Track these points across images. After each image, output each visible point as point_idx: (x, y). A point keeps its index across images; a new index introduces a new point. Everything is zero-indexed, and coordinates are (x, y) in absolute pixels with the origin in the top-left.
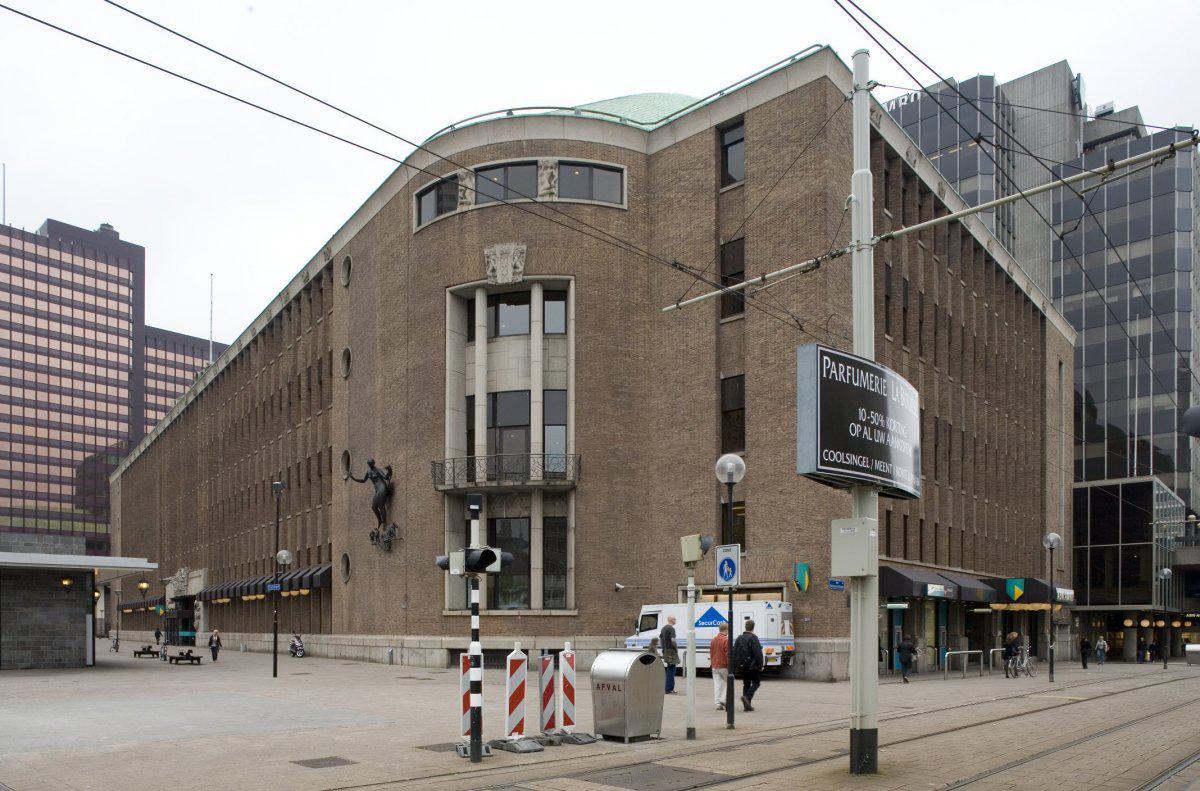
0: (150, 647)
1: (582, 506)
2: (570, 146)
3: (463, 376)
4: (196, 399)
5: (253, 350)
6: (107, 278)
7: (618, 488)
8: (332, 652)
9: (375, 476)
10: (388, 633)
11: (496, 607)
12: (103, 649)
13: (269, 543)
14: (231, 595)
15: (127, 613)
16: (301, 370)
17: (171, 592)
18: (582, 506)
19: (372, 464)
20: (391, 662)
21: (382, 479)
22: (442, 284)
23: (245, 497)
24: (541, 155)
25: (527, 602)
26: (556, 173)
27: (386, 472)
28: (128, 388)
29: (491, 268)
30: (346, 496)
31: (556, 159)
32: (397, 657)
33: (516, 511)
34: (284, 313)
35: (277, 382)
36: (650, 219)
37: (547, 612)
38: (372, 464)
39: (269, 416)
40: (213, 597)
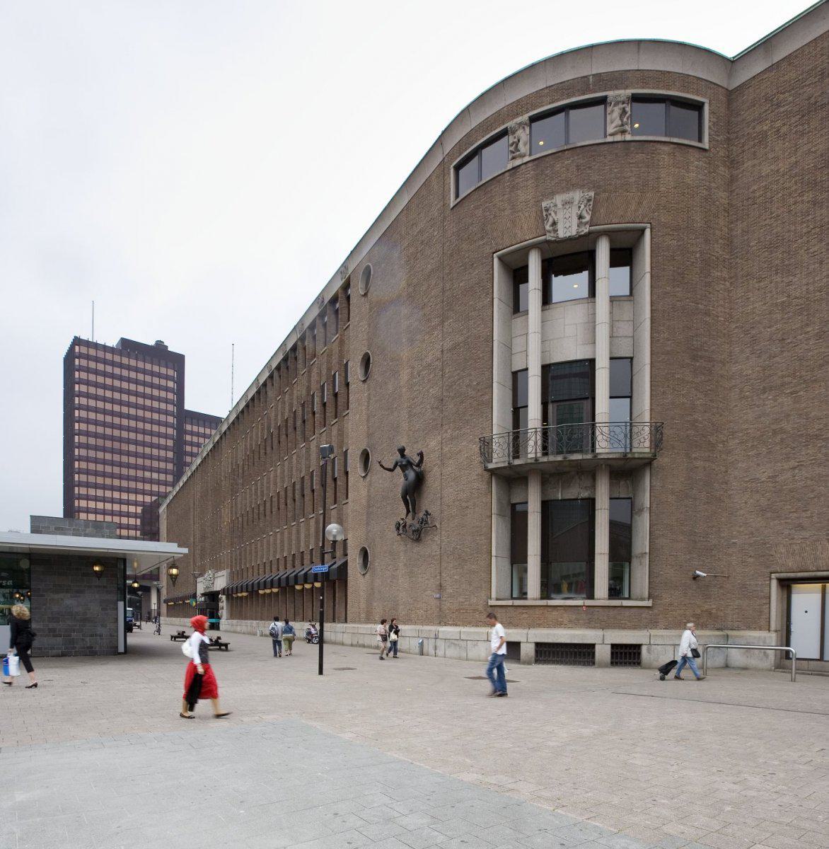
0: (184, 632)
2: (644, 76)
4: (221, 438)
5: (269, 384)
6: (159, 376)
7: (698, 463)
8: (347, 639)
9: (406, 465)
10: (415, 623)
11: (549, 598)
12: (144, 635)
13: (283, 546)
14: (250, 589)
15: (171, 605)
16: (315, 387)
17: (200, 589)
19: (402, 451)
20: (422, 653)
22: (488, 250)
23: (262, 508)
24: (611, 89)
25: (591, 596)
26: (628, 109)
27: (417, 459)
28: (173, 451)
29: (551, 220)
30: (364, 493)
31: (629, 92)
32: (429, 647)
34: (299, 343)
35: (291, 405)
36: (732, 163)
37: (544, 602)
38: (402, 451)
39: (284, 436)
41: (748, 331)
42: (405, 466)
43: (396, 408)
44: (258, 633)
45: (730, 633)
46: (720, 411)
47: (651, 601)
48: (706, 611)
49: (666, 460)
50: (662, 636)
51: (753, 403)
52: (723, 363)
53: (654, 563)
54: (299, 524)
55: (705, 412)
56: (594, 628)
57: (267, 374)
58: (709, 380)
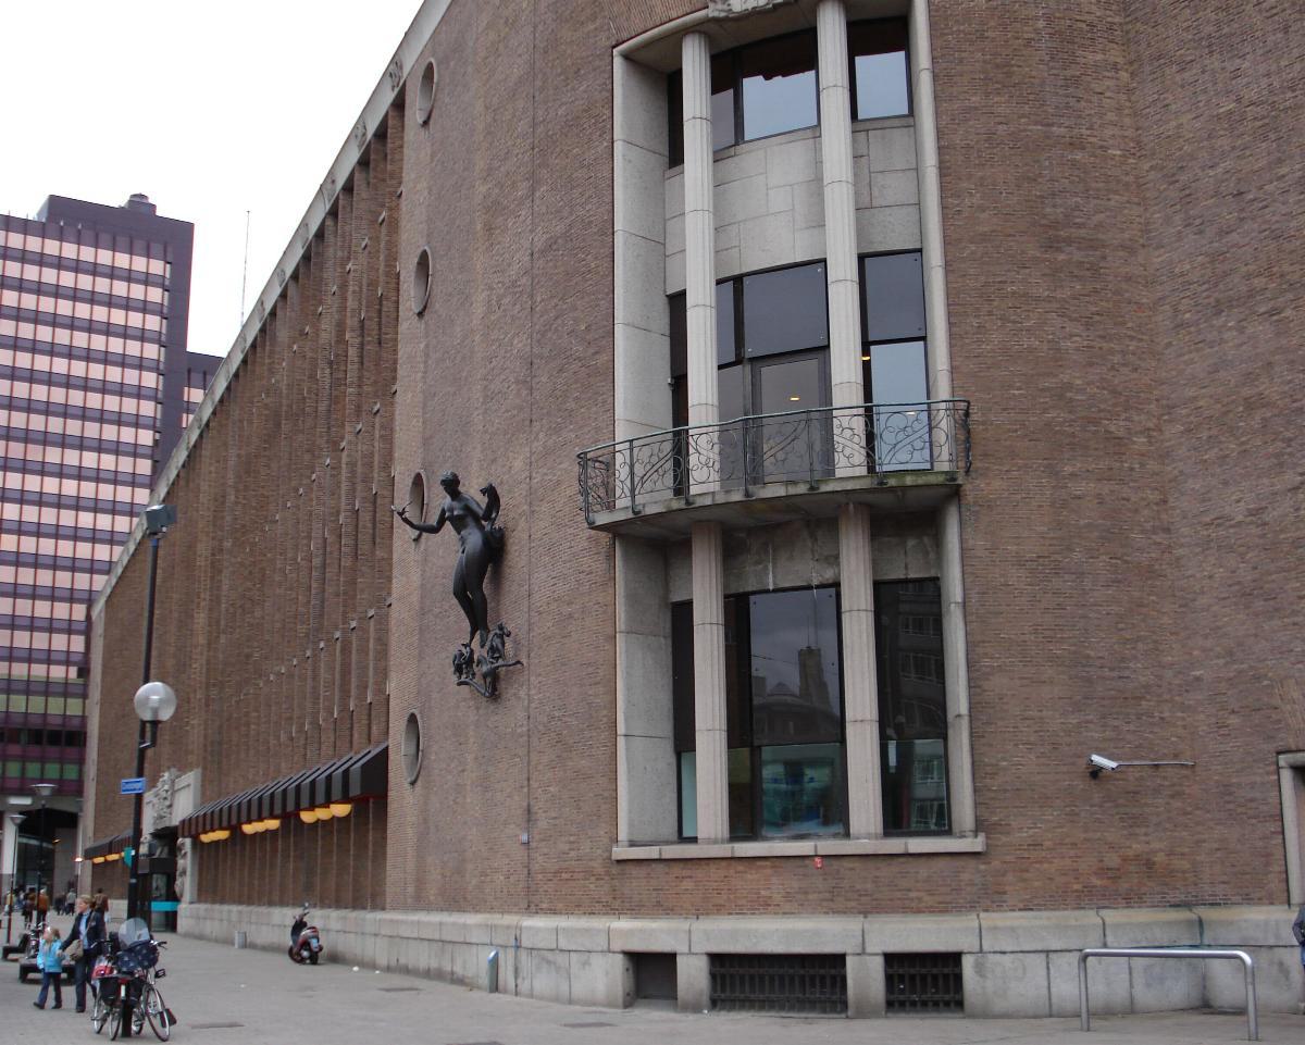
1: (979, 543)
3: (660, 246)
7: (1079, 487)
8: (381, 953)
9: (462, 518)
10: (492, 910)
18: (979, 543)
21: (477, 519)
27: (483, 501)
28: (151, 457)
30: (416, 579)
33: (800, 569)
37: (895, 845)
40: (305, 802)
41: (1174, 175)
42: (459, 517)
43: (466, 378)
44: (237, 939)
45: (1208, 914)
46: (1131, 357)
47: (981, 838)
48: (1137, 857)
49: (996, 484)
50: (1013, 929)
51: (1201, 337)
52: (1130, 249)
53: (983, 741)
54: (317, 652)
55: (1091, 365)
56: (844, 912)
57: (278, 291)
58: (1095, 291)
